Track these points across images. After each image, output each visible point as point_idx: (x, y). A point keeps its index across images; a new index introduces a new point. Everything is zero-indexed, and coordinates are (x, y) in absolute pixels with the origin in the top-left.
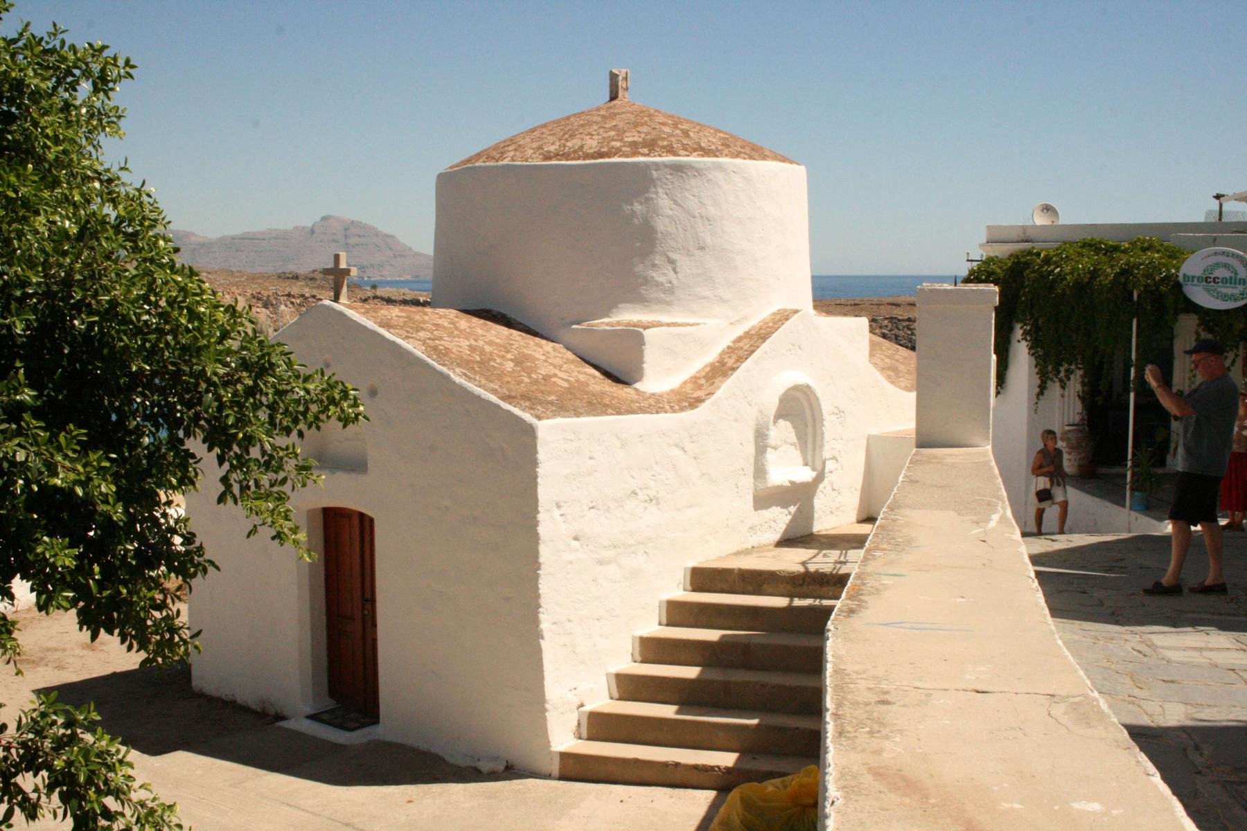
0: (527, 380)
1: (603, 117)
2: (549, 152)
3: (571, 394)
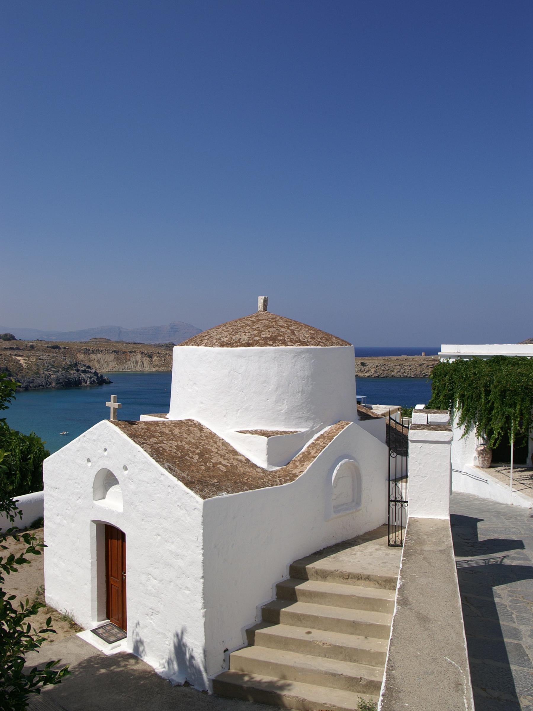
1: (253, 322)
2: (223, 342)
3: (227, 476)
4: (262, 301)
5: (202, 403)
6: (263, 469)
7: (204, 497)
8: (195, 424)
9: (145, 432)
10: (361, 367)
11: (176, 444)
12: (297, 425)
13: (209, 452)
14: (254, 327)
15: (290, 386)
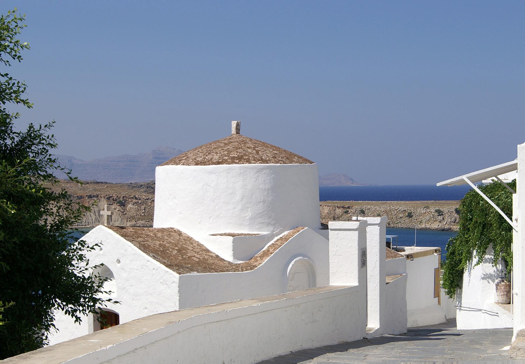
0: (180, 258)
1: (225, 144)
2: (198, 161)
3: (198, 264)
4: (235, 125)
5: (181, 213)
6: (229, 263)
7: (180, 274)
8: (175, 231)
9: (133, 234)
10: (456, 215)
11: (159, 243)
12: (259, 229)
13: (187, 249)
14: (225, 149)
15: (253, 197)
